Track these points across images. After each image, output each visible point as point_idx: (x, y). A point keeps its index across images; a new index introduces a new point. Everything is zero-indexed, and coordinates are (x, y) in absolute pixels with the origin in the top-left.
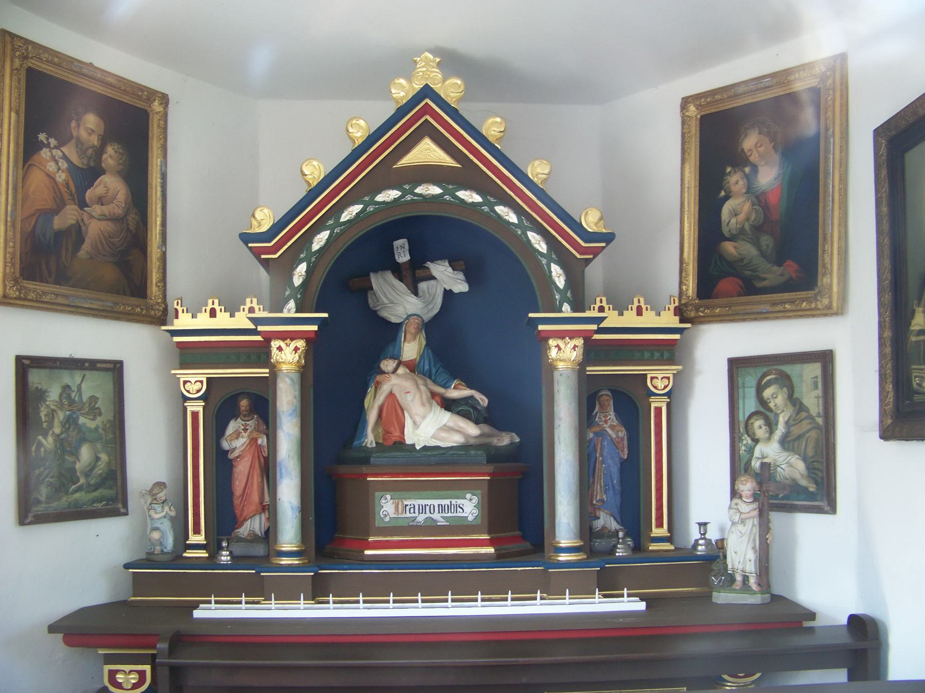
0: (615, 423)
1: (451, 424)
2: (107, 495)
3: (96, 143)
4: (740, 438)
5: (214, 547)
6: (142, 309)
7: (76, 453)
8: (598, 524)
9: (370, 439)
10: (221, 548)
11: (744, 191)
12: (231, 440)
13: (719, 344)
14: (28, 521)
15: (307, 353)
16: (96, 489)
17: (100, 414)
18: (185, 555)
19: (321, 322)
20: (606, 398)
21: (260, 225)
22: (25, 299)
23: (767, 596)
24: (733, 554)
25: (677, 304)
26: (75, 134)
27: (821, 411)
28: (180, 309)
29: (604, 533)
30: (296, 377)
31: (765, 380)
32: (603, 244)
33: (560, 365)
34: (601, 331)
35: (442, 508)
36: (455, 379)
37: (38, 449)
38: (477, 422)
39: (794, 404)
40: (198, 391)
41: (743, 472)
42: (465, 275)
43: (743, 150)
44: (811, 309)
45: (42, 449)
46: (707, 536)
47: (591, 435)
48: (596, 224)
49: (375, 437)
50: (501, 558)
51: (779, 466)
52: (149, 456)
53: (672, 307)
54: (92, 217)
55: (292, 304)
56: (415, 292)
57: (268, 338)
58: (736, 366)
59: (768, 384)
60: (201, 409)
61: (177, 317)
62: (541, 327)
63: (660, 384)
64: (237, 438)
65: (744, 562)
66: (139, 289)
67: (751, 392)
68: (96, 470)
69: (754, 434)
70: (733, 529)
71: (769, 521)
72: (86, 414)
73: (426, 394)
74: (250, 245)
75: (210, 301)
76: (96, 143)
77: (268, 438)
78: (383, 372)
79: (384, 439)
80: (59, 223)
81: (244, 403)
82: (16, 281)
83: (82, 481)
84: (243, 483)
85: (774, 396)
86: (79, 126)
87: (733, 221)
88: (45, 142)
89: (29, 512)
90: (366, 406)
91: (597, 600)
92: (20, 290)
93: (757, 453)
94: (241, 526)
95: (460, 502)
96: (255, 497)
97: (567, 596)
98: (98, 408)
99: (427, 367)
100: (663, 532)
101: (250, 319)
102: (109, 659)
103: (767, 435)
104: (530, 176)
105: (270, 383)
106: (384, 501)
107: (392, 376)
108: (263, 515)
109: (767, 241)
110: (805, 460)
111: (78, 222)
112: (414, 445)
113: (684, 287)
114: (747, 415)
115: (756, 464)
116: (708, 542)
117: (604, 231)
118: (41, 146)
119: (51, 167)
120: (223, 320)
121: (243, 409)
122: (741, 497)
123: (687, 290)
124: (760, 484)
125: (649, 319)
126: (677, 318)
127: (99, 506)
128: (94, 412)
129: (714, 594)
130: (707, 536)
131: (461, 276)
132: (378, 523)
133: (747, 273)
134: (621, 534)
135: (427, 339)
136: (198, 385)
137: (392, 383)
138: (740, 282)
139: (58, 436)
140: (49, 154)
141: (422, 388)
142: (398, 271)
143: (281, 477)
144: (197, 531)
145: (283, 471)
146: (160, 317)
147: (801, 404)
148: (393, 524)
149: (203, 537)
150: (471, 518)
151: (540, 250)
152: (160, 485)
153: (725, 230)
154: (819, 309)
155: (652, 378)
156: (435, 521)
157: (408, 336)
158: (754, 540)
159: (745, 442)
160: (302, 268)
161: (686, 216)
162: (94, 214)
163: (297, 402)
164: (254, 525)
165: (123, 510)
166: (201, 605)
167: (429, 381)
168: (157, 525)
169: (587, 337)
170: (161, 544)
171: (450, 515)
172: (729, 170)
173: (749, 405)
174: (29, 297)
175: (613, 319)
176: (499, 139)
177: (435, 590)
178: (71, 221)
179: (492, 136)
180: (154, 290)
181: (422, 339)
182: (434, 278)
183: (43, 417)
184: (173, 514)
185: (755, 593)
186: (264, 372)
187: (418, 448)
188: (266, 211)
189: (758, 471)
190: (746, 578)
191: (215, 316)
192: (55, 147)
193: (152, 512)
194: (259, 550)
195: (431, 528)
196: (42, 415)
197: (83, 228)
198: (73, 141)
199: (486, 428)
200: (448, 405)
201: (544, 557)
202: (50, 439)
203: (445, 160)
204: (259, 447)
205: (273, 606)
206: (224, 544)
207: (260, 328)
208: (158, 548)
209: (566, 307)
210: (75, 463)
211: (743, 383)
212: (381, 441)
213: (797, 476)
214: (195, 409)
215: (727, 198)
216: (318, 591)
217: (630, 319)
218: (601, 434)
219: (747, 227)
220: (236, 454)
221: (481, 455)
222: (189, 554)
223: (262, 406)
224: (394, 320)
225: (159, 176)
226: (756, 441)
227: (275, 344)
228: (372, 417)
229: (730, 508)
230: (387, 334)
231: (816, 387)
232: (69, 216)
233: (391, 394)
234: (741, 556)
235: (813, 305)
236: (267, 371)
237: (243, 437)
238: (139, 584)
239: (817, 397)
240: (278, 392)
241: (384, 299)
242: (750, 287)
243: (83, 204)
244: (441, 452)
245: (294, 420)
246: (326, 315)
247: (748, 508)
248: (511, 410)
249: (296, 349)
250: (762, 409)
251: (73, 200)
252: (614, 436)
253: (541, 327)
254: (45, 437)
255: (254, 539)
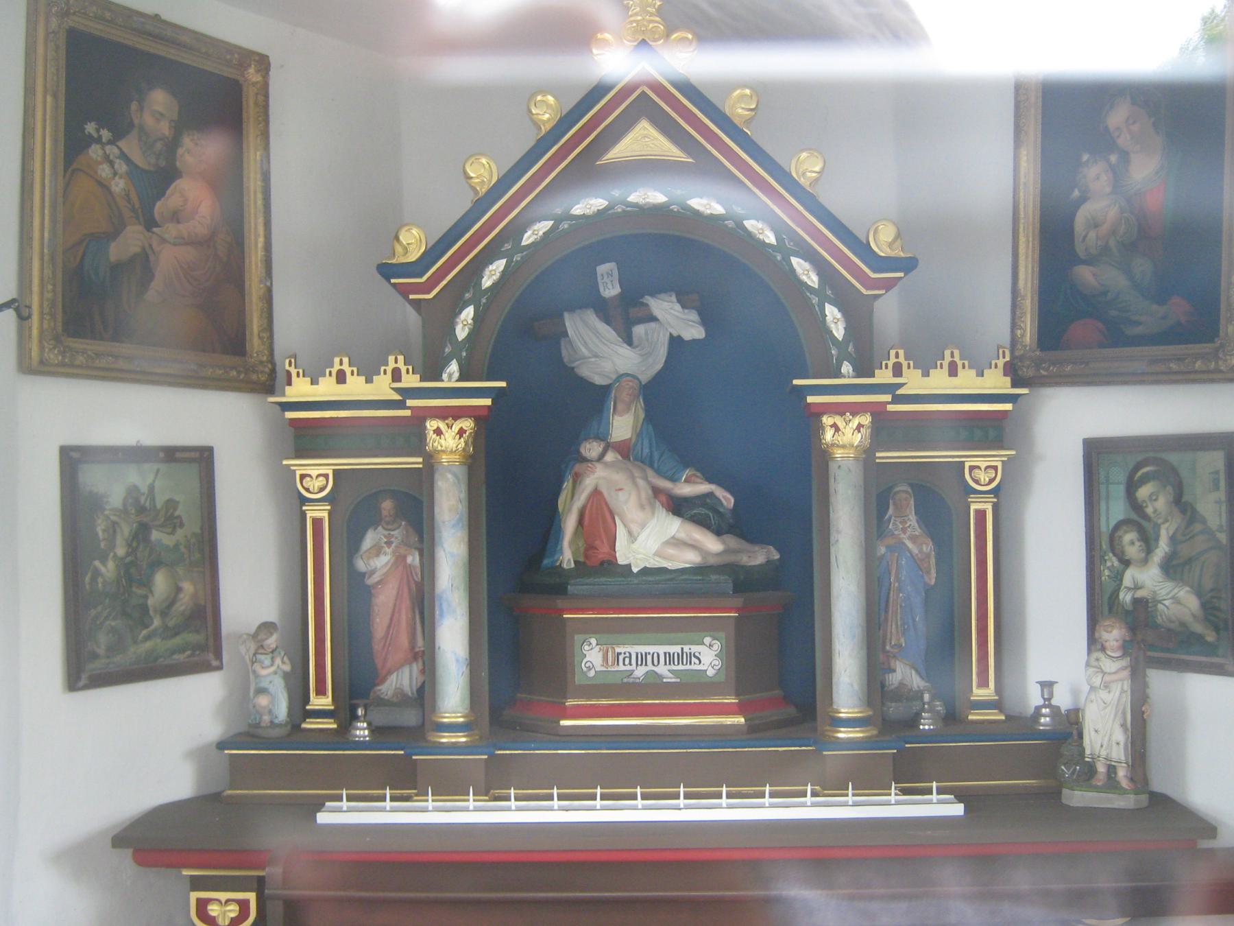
0: (918, 532)
1: (682, 535)
2: (195, 641)
3: (167, 133)
4: (1102, 557)
5: (345, 714)
6: (239, 372)
7: (147, 584)
8: (894, 679)
9: (567, 557)
10: (355, 717)
11: (1108, 190)
12: (369, 558)
13: (1074, 417)
14: (81, 684)
15: (476, 435)
16: (176, 634)
17: (182, 525)
18: (304, 726)
19: (496, 394)
20: (904, 495)
21: (406, 251)
22: (72, 366)
23: (1144, 798)
24: (1093, 733)
25: (1008, 358)
26: (136, 122)
27: (1224, 524)
28: (294, 372)
29: (902, 694)
30: (462, 471)
31: (1139, 474)
32: (902, 275)
33: (838, 453)
34: (898, 399)
35: (670, 658)
36: (686, 466)
37: (94, 579)
38: (718, 533)
39: (1183, 512)
40: (322, 489)
41: (1106, 609)
42: (700, 314)
43: (1106, 129)
44: (1209, 372)
45: (100, 580)
46: (1054, 702)
47: (883, 550)
48: (890, 245)
49: (574, 554)
50: (754, 731)
51: (1160, 602)
52: (250, 589)
53: (1001, 362)
54: (163, 240)
55: (454, 367)
56: (629, 340)
57: (420, 416)
58: (1097, 453)
59: (1144, 480)
60: (325, 515)
61: (289, 383)
62: (811, 399)
63: (983, 477)
64: (378, 555)
65: (1110, 746)
66: (236, 344)
67: (1119, 491)
68: (177, 605)
69: (1123, 552)
70: (1093, 697)
71: (1145, 685)
72: (162, 526)
73: (646, 492)
74: (393, 281)
75: (337, 360)
76: (167, 133)
77: (421, 555)
78: (585, 460)
79: (586, 557)
80: (117, 251)
81: (387, 505)
82: (57, 339)
83: (157, 622)
84: (386, 621)
85: (1153, 498)
86: (141, 109)
87: (1092, 235)
88: (95, 135)
89: (85, 669)
90: (560, 508)
91: (893, 798)
92: (63, 353)
93: (1127, 580)
94: (383, 681)
95: (695, 649)
96: (404, 640)
97: (850, 791)
98: (179, 517)
99: (646, 450)
100: (985, 693)
101: (396, 390)
102: (197, 884)
103: (1143, 555)
104: (794, 175)
105: (426, 476)
106: (587, 648)
107: (599, 466)
108: (415, 666)
109: (1142, 267)
110: (1199, 594)
111: (143, 249)
112: (629, 566)
113: (1019, 332)
114: (1113, 523)
115: (1126, 597)
116: (1055, 711)
117: (902, 255)
118: (90, 140)
119: (104, 171)
120: (356, 388)
121: (385, 513)
122: (1103, 649)
123: (1023, 336)
124: (1133, 629)
125: (967, 382)
126: (1008, 379)
127: (180, 658)
128: (172, 522)
129: (1065, 791)
130: (1054, 702)
131: (694, 316)
132: (578, 680)
133: (1113, 313)
134: (927, 697)
135: (647, 411)
136: (322, 481)
137: (596, 475)
138: (1100, 325)
139: (122, 559)
140: (100, 152)
141: (641, 482)
142: (603, 309)
143: (441, 615)
144: (321, 691)
145: (445, 606)
146: (265, 381)
147: (1194, 511)
148: (598, 682)
149: (330, 699)
150: (711, 673)
151: (809, 283)
152: (267, 627)
153: (1080, 249)
154: (1221, 372)
155: (972, 468)
156: (660, 676)
157: (620, 406)
158: (1124, 713)
159: (1109, 564)
160: (468, 313)
161: (1021, 226)
162: (166, 236)
163: (462, 508)
164: (402, 680)
165: (215, 663)
166: (328, 804)
167: (650, 473)
168: (264, 684)
169: (878, 412)
170: (270, 712)
171: (681, 667)
172: (1085, 157)
173: (1116, 510)
174: (77, 362)
175: (914, 382)
176: (749, 121)
177: (659, 782)
178: (135, 249)
179: (740, 116)
180: (255, 343)
181: (639, 408)
182: (653, 319)
183: (100, 533)
184: (287, 668)
185: (1123, 792)
186: (415, 462)
187: (635, 570)
188: (415, 231)
189: (1130, 608)
190: (1112, 770)
191: (344, 382)
192: (110, 142)
193: (257, 667)
194: (409, 718)
195: (654, 686)
196: (99, 530)
197: (152, 258)
198: (135, 132)
199: (733, 542)
200: (678, 507)
201: (815, 730)
202: (111, 565)
203: (670, 150)
204: (409, 569)
205: (430, 805)
206: (360, 712)
207: (409, 403)
208: (266, 718)
209: (846, 368)
210: (146, 597)
211: (1107, 478)
212: (582, 559)
213: (1188, 619)
214: (318, 514)
215: (1083, 199)
216: (492, 785)
217: (939, 382)
218: (899, 547)
219: (1112, 243)
220: (376, 578)
221: (726, 583)
222: (310, 724)
223: (412, 505)
224: (599, 380)
225: (259, 176)
226: (1126, 563)
227: (432, 425)
228: (570, 524)
229: (1088, 665)
230: (592, 401)
231: (1217, 488)
232: (131, 240)
233: (596, 493)
234: (1104, 736)
235: (1212, 365)
236: (420, 460)
237: (385, 554)
238: (239, 771)
239: (1218, 502)
240: (437, 494)
241: (584, 350)
242: (1117, 334)
243: (150, 223)
244: (668, 576)
245: (459, 534)
246: (503, 384)
247: (1113, 665)
248: (771, 508)
249: (461, 432)
250: (1134, 516)
251: (138, 218)
252: (915, 551)
253: (810, 399)
254: (104, 562)
255: (402, 701)
